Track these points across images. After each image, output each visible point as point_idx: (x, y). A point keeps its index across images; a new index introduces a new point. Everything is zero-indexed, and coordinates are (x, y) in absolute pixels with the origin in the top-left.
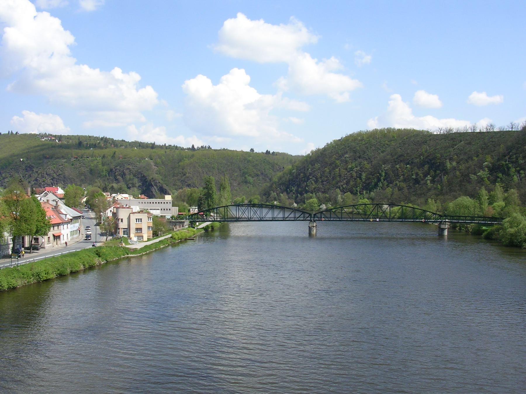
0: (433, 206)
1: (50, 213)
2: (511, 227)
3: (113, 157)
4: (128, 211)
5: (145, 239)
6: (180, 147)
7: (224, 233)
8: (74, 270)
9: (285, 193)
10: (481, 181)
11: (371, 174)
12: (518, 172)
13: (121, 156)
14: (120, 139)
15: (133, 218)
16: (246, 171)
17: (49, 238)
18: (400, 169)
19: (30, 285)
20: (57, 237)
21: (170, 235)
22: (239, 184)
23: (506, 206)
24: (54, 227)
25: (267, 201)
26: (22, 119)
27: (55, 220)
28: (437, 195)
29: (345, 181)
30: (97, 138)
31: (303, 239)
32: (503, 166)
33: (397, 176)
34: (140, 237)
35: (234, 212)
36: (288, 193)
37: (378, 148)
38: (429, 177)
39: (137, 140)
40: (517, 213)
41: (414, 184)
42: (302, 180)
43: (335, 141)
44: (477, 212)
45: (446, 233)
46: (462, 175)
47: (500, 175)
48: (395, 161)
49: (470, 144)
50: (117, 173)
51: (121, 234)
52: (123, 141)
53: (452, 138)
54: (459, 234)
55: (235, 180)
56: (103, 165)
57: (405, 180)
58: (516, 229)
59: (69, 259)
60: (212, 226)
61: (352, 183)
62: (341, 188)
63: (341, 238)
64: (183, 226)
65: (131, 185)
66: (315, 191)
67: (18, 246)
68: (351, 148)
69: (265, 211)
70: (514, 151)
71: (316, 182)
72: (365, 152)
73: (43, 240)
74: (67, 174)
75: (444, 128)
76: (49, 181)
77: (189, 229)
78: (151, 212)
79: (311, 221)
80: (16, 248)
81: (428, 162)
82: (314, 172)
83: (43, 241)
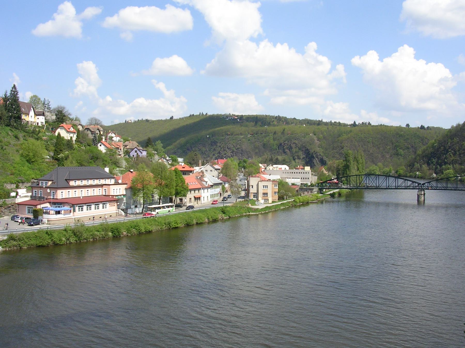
3: (283, 133)
5: (270, 201)
8: (199, 222)
13: (289, 132)
14: (293, 118)
15: (261, 184)
16: (397, 144)
21: (293, 200)
22: (391, 156)
24: (191, 191)
30: (273, 117)
31: (413, 206)
34: (266, 200)
36: (428, 164)
42: (442, 153)
52: (294, 119)
55: (388, 153)
56: (274, 140)
65: (296, 157)
71: (454, 154)
74: (244, 148)
76: (229, 154)
82: (453, 145)
83: (186, 201)
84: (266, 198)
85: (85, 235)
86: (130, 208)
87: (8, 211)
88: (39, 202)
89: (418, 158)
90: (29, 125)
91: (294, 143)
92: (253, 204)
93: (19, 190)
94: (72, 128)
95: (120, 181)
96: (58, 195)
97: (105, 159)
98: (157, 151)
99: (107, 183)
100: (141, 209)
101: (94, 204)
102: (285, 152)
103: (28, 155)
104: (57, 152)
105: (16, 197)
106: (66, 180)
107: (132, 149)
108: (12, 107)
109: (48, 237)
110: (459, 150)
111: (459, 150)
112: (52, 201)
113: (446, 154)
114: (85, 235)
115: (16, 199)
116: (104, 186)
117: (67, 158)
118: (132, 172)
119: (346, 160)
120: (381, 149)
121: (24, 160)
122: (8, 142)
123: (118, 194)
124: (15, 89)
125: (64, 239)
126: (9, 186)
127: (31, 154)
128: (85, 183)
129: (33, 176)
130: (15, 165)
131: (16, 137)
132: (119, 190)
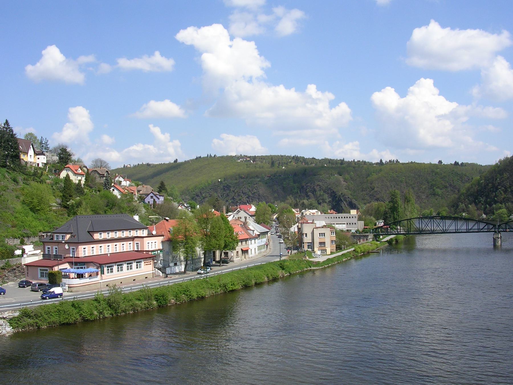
1: (238, 230)
4: (312, 226)
5: (329, 252)
6: (369, 162)
7: (409, 246)
8: (258, 282)
9: (473, 205)
14: (311, 157)
15: (317, 232)
16: (434, 183)
17: (237, 252)
19: (218, 295)
20: (245, 252)
21: (353, 249)
22: (427, 197)
25: (455, 213)
26: (221, 142)
27: (242, 235)
30: (289, 157)
31: (487, 252)
34: (324, 251)
36: (476, 204)
51: (306, 248)
52: (313, 158)
55: (423, 193)
59: (253, 272)
60: (396, 239)
64: (367, 240)
65: (321, 201)
66: (504, 201)
67: (210, 260)
69: (448, 222)
71: (505, 191)
73: (232, 254)
76: (245, 199)
77: (373, 242)
78: (337, 226)
79: (495, 232)
80: (207, 262)
82: (503, 181)
83: (232, 255)
85: (123, 306)
86: (169, 266)
87: (13, 275)
88: (56, 262)
89: (463, 197)
90: (28, 165)
93: (24, 247)
94: (79, 169)
95: (154, 233)
96: (80, 252)
97: (122, 205)
98: (172, 196)
99: (138, 235)
100: (183, 267)
101: (124, 264)
102: (308, 196)
103: (31, 202)
104: (66, 198)
105: (22, 255)
106: (89, 232)
107: (148, 195)
108: (9, 144)
109: (75, 311)
110: (510, 187)
111: (510, 187)
112: (74, 260)
114: (123, 306)
115: (23, 259)
116: (136, 239)
117: (79, 204)
118: (167, 220)
119: (392, 202)
120: (416, 189)
121: (28, 208)
122: (5, 187)
123: (153, 249)
124: (8, 125)
125: (96, 313)
126: (12, 242)
127: (35, 201)
128: (112, 235)
129: (41, 228)
130: (17, 215)
131: (15, 180)
132: (154, 244)
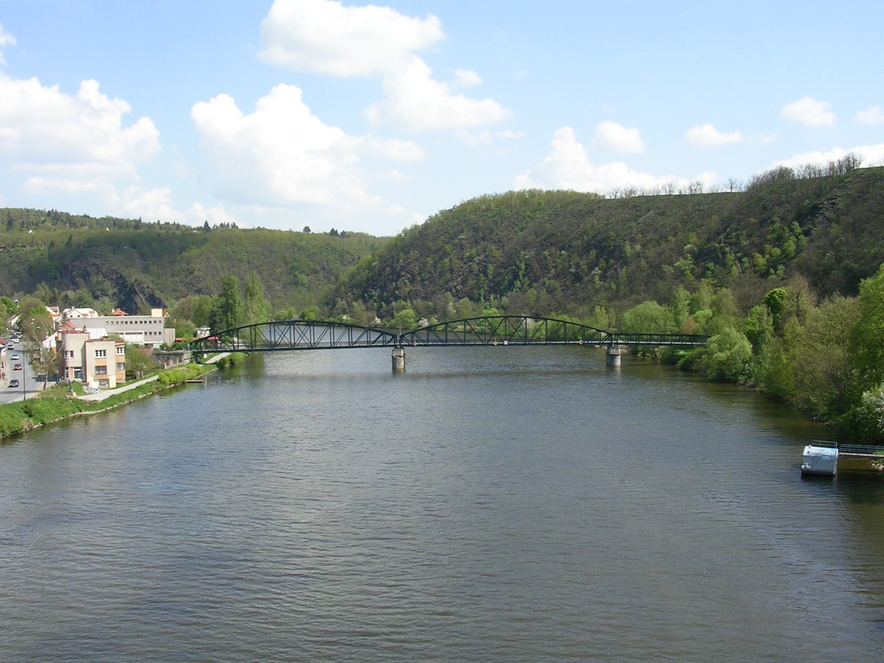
0: (602, 319)
2: (721, 350)
5: (113, 384)
7: (254, 372)
9: (360, 301)
10: (680, 275)
11: (504, 266)
12: (740, 260)
14: (82, 214)
15: (91, 349)
16: (295, 264)
18: (549, 258)
21: (156, 377)
22: (284, 287)
23: (714, 315)
25: (331, 315)
28: (610, 300)
29: (459, 279)
30: (41, 213)
31: (384, 379)
32: (715, 250)
33: (545, 268)
34: (104, 382)
35: (266, 335)
36: (365, 301)
37: (514, 223)
38: (597, 271)
39: (110, 215)
40: (730, 327)
41: (574, 282)
43: (442, 212)
44: (670, 327)
45: (618, 362)
46: (651, 267)
47: (711, 265)
48: (542, 245)
49: (663, 214)
50: (75, 273)
51: (71, 377)
52: (85, 216)
53: (635, 206)
54: (641, 363)
55: (278, 281)
57: (557, 277)
58: (728, 353)
61: (471, 282)
62: (454, 291)
63: (446, 376)
65: (99, 293)
66: (410, 296)
68: (469, 224)
69: (319, 330)
70: (733, 226)
71: (412, 281)
72: (492, 230)
75: (622, 189)
77: (191, 365)
79: (395, 346)
81: (595, 246)
82: (409, 264)
84: (104, 377)
89: (343, 289)
91: (94, 264)
92: (80, 392)
113: (396, 281)
120: (265, 273)
